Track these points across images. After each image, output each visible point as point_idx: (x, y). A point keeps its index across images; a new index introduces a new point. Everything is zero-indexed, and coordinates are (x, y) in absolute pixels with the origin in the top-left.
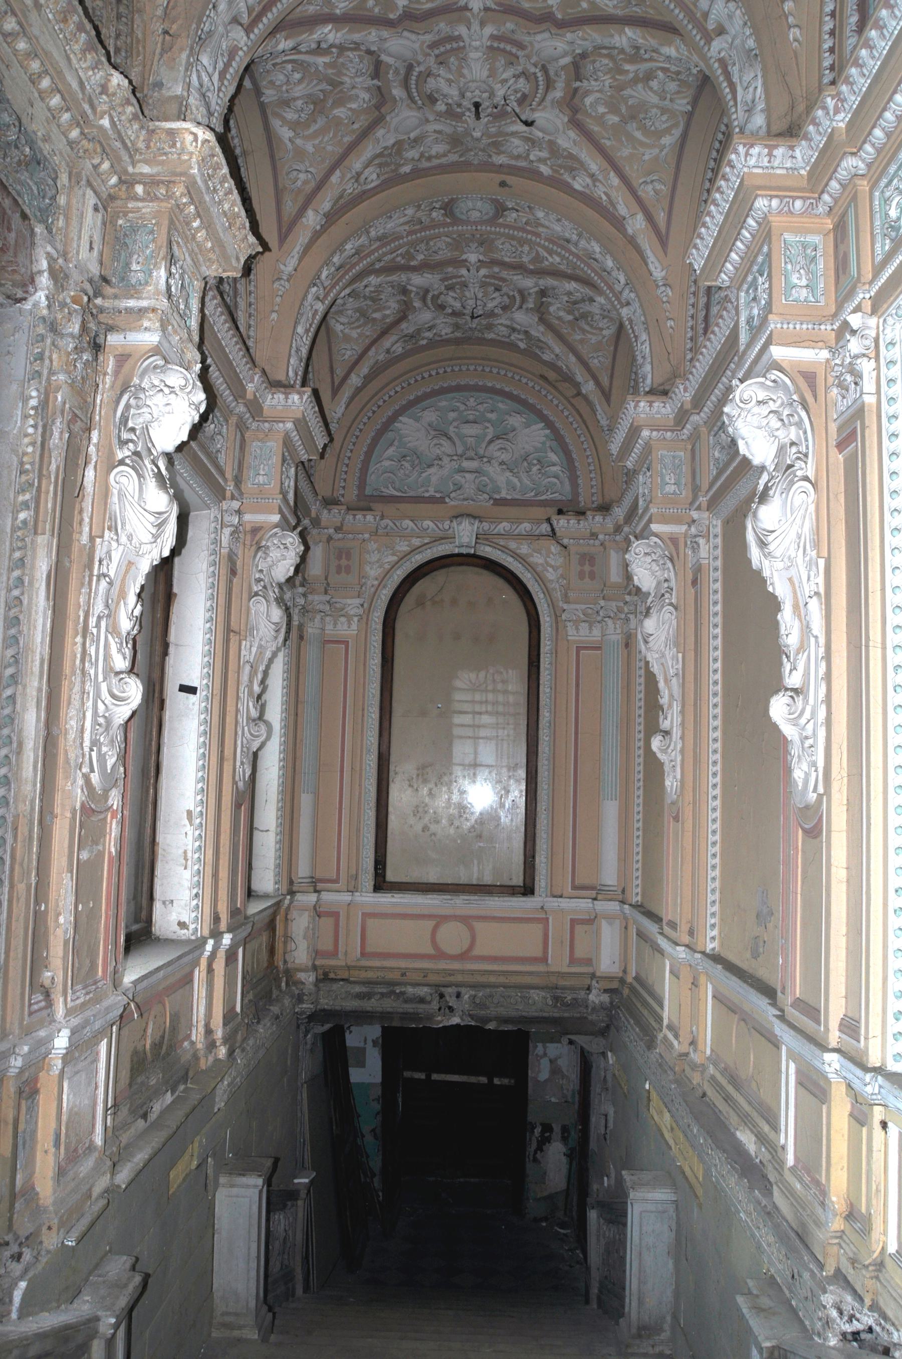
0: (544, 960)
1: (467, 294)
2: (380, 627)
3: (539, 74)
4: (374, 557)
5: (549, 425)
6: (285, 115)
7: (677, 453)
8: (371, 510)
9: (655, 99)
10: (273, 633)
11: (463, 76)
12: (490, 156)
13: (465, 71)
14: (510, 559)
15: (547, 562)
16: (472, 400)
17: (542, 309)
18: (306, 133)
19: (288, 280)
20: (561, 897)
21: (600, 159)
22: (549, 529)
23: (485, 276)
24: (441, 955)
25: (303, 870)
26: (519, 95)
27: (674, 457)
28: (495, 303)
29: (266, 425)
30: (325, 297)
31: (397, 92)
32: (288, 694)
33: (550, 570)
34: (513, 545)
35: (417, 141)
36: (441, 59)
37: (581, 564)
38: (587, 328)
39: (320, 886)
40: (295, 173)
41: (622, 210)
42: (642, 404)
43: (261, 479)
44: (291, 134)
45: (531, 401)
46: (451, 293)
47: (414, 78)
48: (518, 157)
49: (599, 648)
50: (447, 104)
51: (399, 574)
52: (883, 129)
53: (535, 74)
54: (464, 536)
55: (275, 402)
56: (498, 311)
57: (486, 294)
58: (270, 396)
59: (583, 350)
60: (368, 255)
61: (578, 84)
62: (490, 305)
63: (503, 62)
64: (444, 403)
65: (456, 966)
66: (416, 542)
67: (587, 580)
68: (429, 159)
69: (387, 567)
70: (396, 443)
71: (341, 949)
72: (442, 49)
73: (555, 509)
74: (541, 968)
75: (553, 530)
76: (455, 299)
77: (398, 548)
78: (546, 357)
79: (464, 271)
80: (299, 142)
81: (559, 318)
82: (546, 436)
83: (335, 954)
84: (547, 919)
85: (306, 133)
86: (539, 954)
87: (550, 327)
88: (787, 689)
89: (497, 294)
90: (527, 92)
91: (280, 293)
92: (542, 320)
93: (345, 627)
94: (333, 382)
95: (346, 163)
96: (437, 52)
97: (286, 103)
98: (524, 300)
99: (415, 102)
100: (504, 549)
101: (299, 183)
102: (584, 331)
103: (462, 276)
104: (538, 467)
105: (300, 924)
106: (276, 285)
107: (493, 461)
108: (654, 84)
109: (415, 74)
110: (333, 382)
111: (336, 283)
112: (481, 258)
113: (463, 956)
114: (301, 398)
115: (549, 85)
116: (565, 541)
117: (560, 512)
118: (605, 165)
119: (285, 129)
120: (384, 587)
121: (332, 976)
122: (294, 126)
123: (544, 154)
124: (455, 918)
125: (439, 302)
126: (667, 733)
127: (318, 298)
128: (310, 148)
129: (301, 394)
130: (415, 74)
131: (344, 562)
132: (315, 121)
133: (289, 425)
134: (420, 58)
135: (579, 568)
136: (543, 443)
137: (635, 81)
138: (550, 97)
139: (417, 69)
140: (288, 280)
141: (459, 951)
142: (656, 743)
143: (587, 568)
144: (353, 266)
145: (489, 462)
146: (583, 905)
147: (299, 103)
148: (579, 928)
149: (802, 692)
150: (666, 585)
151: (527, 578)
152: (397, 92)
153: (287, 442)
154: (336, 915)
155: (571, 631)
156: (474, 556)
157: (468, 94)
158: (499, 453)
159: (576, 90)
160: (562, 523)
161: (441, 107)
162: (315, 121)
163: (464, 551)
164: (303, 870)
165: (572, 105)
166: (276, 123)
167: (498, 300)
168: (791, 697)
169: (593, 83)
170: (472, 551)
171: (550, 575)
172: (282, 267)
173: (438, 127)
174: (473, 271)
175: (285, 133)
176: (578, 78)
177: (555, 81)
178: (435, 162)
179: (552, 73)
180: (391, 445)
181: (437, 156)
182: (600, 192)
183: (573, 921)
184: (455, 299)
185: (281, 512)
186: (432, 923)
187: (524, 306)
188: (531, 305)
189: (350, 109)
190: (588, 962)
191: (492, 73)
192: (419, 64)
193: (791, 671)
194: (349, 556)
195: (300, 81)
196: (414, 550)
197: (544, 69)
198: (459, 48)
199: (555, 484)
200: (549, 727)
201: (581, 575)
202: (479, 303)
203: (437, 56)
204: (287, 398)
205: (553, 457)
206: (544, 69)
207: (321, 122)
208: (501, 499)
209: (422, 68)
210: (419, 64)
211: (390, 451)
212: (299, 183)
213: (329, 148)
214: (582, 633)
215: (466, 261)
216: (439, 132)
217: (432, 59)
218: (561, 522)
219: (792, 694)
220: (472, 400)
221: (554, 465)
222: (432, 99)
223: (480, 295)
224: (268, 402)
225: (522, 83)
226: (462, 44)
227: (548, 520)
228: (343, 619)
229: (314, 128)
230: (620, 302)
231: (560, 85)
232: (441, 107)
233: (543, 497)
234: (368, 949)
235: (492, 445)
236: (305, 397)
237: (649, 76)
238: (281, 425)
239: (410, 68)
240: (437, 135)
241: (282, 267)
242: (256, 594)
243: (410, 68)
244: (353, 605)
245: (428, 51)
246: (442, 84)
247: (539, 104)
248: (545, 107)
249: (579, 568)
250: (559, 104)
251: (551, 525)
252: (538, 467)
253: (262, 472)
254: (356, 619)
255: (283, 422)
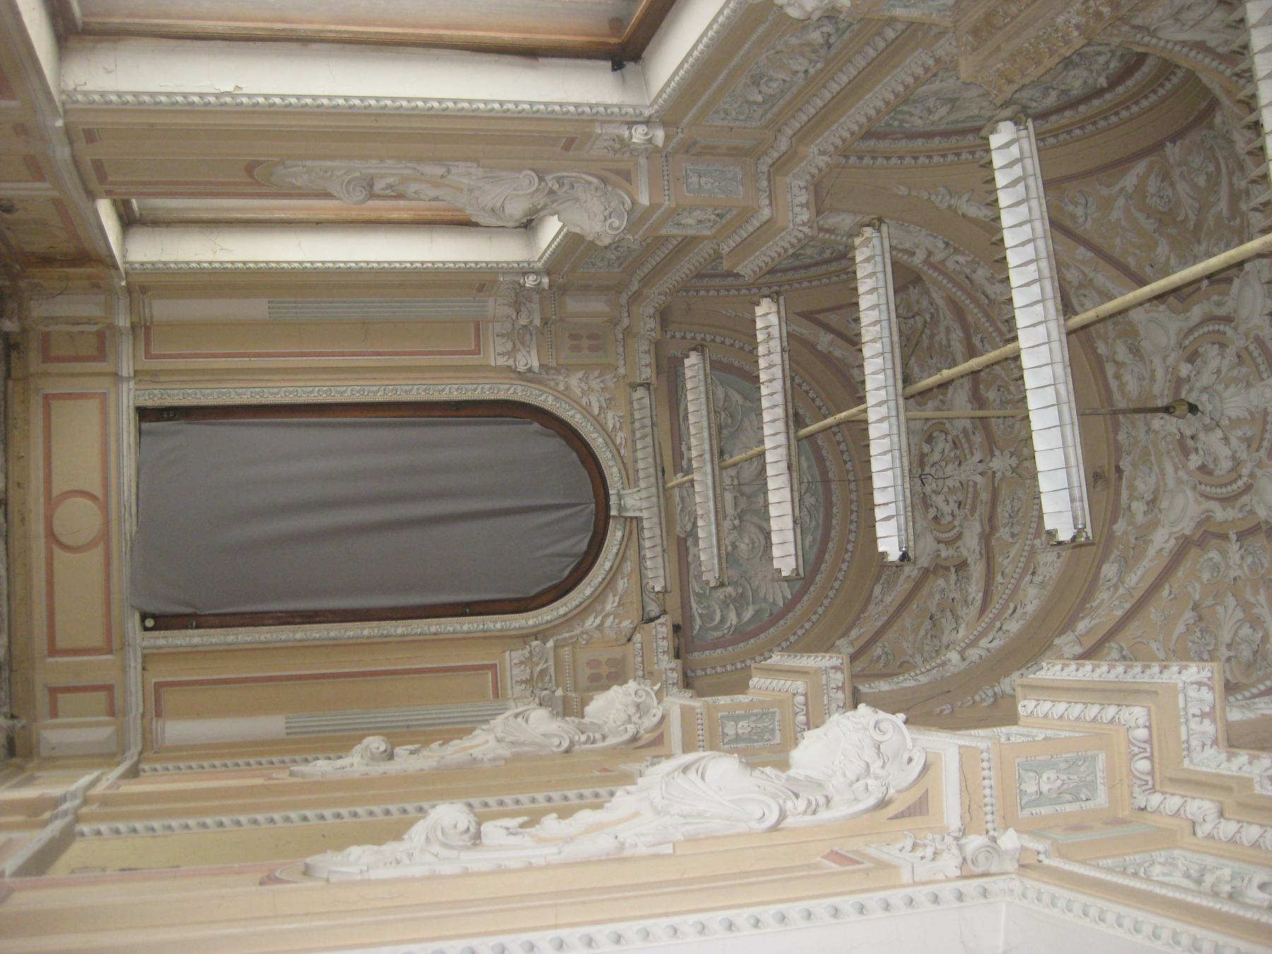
0: (53, 651)
1: (950, 466)
2: (502, 396)
3: (1240, 483)
4: (595, 384)
5: (790, 606)
6: (1153, 175)
7: (778, 734)
8: (658, 374)
9: (1226, 636)
10: (490, 205)
11: (1227, 387)
12: (1129, 454)
13: (1232, 389)
14: (608, 565)
15: (608, 615)
16: (813, 500)
17: (941, 571)
18: (1132, 208)
19: (950, 206)
20: (144, 669)
21: (1144, 586)
22: (653, 614)
23: (975, 484)
24: (51, 503)
25: (162, 310)
26: (1212, 466)
27: (773, 730)
28: (942, 505)
29: (765, 183)
30: (932, 266)
31: (1196, 313)
32: (430, 114)
33: (598, 621)
34: (628, 567)
35: (1136, 351)
36: (1244, 354)
37: (610, 662)
38: (922, 632)
39: (141, 333)
40: (1082, 201)
41: (1082, 626)
42: (839, 676)
43: (694, 179)
44: (1130, 190)
45: (818, 578)
46: (948, 446)
47: (1216, 327)
48: (1132, 488)
49: (496, 695)
50: (1189, 377)
51: (574, 418)
52: (1238, 832)
53: (1240, 477)
54: (633, 500)
55: (796, 191)
56: (932, 512)
57: (952, 491)
58: (803, 184)
59: (891, 634)
60: (989, 318)
61: (1233, 537)
62: (939, 500)
63: (1249, 433)
64: (805, 464)
65: (37, 527)
66: (620, 437)
67: (588, 671)
68: (1117, 377)
69: (584, 401)
70: (748, 404)
71: (55, 367)
72: (1256, 354)
73: (679, 621)
74: (41, 643)
75: (652, 620)
76: (943, 452)
77: (610, 415)
78: (877, 589)
79: (977, 457)
80: (1121, 201)
81: (931, 595)
82: (774, 603)
83: (47, 359)
84: (110, 652)
85: (1132, 208)
86: (61, 643)
87: (918, 585)
88: (479, 824)
89: (953, 506)
90: (1217, 472)
91: (933, 197)
92: (926, 573)
93: (499, 349)
94: (819, 312)
95: (1101, 262)
96: (1252, 348)
97: (1166, 176)
98: (948, 543)
99: (1186, 336)
100: (621, 558)
101: (1071, 208)
102: (916, 630)
103: (972, 454)
104: (734, 594)
105: (87, 307)
106: (941, 190)
107: (735, 534)
108: (1246, 631)
109: (1222, 328)
110: (819, 312)
111: (951, 280)
112: (998, 475)
113: (51, 535)
114: (804, 224)
115: (1226, 501)
116: (637, 637)
117: (677, 628)
118: (1137, 595)
119: (1135, 181)
120: (556, 399)
121: (14, 354)
122: (1140, 190)
123: (1140, 519)
124: (107, 522)
125: (935, 434)
126: (390, 756)
127: (930, 253)
128: (1114, 216)
129: (808, 224)
130: (1222, 328)
131: (585, 343)
132: (1148, 217)
133: (766, 213)
134: (1242, 328)
135: (603, 659)
136: (765, 599)
137: (1246, 606)
138: (1214, 505)
139: (1227, 328)
140: (950, 206)
141: (57, 529)
142: (376, 743)
143: (604, 670)
144: (975, 300)
145: (735, 527)
146: (135, 702)
147: (1169, 192)
148: (101, 696)
149: (475, 845)
150: (598, 736)
151: (585, 589)
152: (1196, 313)
153: (747, 213)
154: (101, 356)
155: (518, 655)
156: (608, 517)
157: (1205, 397)
158: (746, 540)
159: (1225, 537)
160: (662, 629)
161: (1185, 370)
162: (1148, 217)
163: (613, 500)
164: (162, 310)
165: (1204, 536)
166: (1140, 167)
167: (947, 510)
168: (468, 829)
169: (1237, 556)
170: (613, 512)
171: (591, 622)
172: (965, 197)
173: (1160, 374)
174: (981, 468)
175: (1130, 181)
176: (1241, 536)
177: (1233, 508)
178: (1114, 385)
179: (1245, 499)
180: (745, 398)
181: (1122, 386)
182: (1103, 595)
183: (109, 688)
184: (943, 452)
185: (653, 207)
186: (98, 492)
187: (942, 546)
188: (944, 554)
189: (1168, 259)
190: (54, 714)
191: (1235, 423)
192: (1235, 329)
193: (507, 829)
194: (594, 349)
195: (1194, 186)
196: (609, 437)
197: (1248, 488)
198: (1260, 373)
199: (712, 620)
200: (382, 636)
201: (593, 663)
202: (940, 482)
203: (1246, 348)
204: (802, 206)
205: (748, 614)
206: (1248, 488)
207: (1148, 225)
208: (687, 549)
209: (1230, 332)
210: (1235, 329)
211: (737, 398)
212: (1071, 208)
213: (1118, 241)
214: (516, 671)
215: (993, 455)
216: (1153, 379)
217: (1242, 343)
218: (664, 629)
219: (473, 830)
220: (813, 500)
221: (739, 615)
222: (1192, 358)
223: (950, 483)
224: (796, 183)
225: (1226, 464)
226: (1265, 375)
227: (664, 612)
228: (509, 346)
229: (1140, 217)
230: (964, 649)
231: (1231, 514)
232: (1185, 370)
233: (694, 606)
234: (54, 404)
235: (757, 531)
236: (806, 229)
237: (1256, 622)
238: (767, 202)
239: (1228, 320)
240: (1147, 376)
241: (965, 197)
242: (541, 179)
243: (1228, 320)
244: (529, 359)
245: (1252, 335)
246: (1214, 363)
247: (1202, 495)
248: (1199, 503)
249: (603, 659)
250: (1207, 518)
251: (658, 617)
252: (734, 594)
253: (703, 180)
254: (511, 362)
255: (771, 204)
